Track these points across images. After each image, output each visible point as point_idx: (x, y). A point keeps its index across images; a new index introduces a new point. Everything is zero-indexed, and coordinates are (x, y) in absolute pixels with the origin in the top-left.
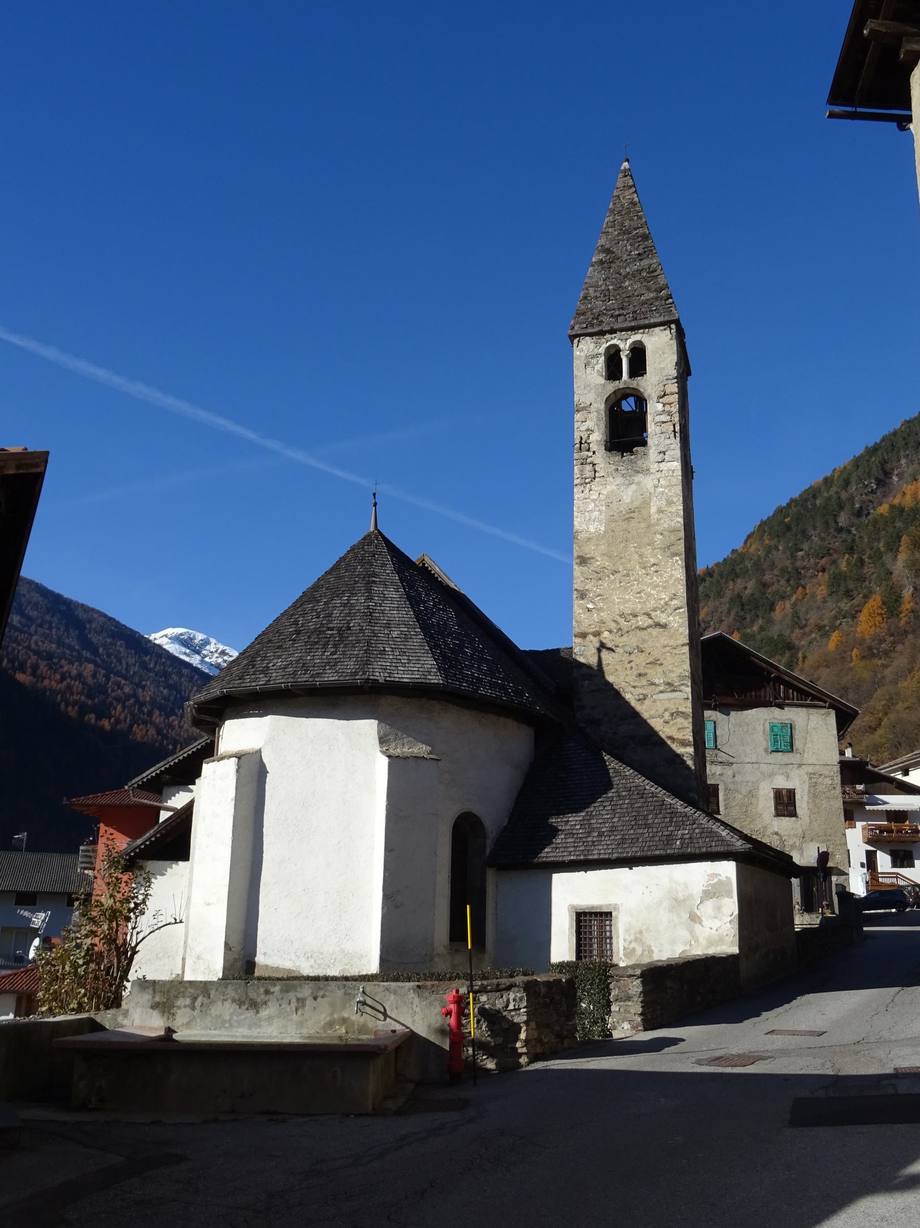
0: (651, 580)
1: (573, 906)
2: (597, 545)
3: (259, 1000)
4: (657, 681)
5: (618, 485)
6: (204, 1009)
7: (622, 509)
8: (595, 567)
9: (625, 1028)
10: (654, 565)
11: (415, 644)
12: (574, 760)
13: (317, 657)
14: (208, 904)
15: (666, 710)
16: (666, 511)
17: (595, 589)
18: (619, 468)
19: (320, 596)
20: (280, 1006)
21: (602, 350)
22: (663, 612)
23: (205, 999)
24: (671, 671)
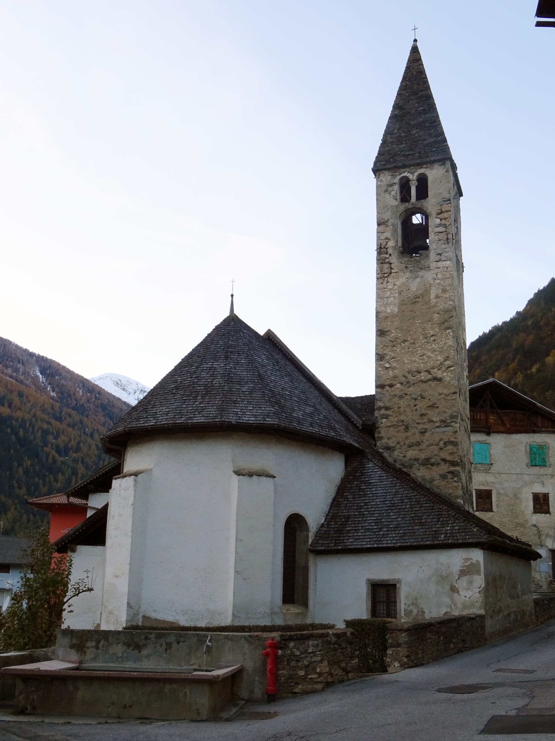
0: (431, 346)
1: (369, 579)
2: (392, 322)
3: (141, 644)
4: (435, 419)
5: (407, 278)
6: (105, 649)
7: (410, 295)
8: (391, 338)
9: (396, 666)
10: (433, 335)
11: (259, 396)
12: (372, 476)
13: (190, 406)
14: (117, 576)
15: (441, 440)
16: (442, 297)
17: (390, 353)
18: (409, 266)
19: (193, 362)
20: (155, 647)
21: (397, 180)
22: (439, 370)
23: (105, 642)
24: (444, 412)
